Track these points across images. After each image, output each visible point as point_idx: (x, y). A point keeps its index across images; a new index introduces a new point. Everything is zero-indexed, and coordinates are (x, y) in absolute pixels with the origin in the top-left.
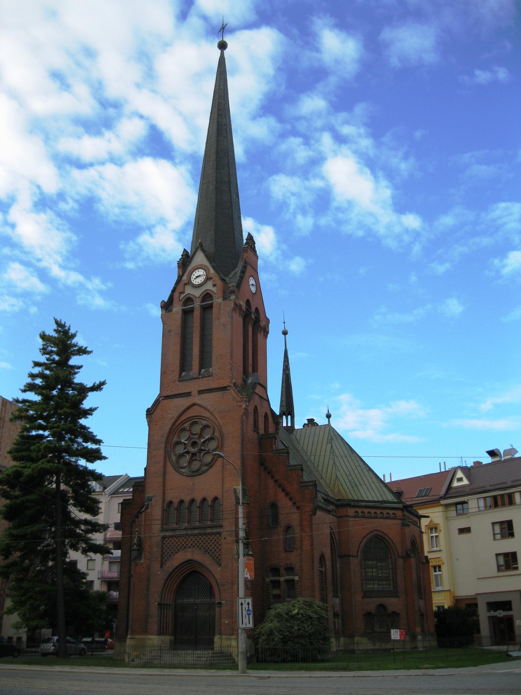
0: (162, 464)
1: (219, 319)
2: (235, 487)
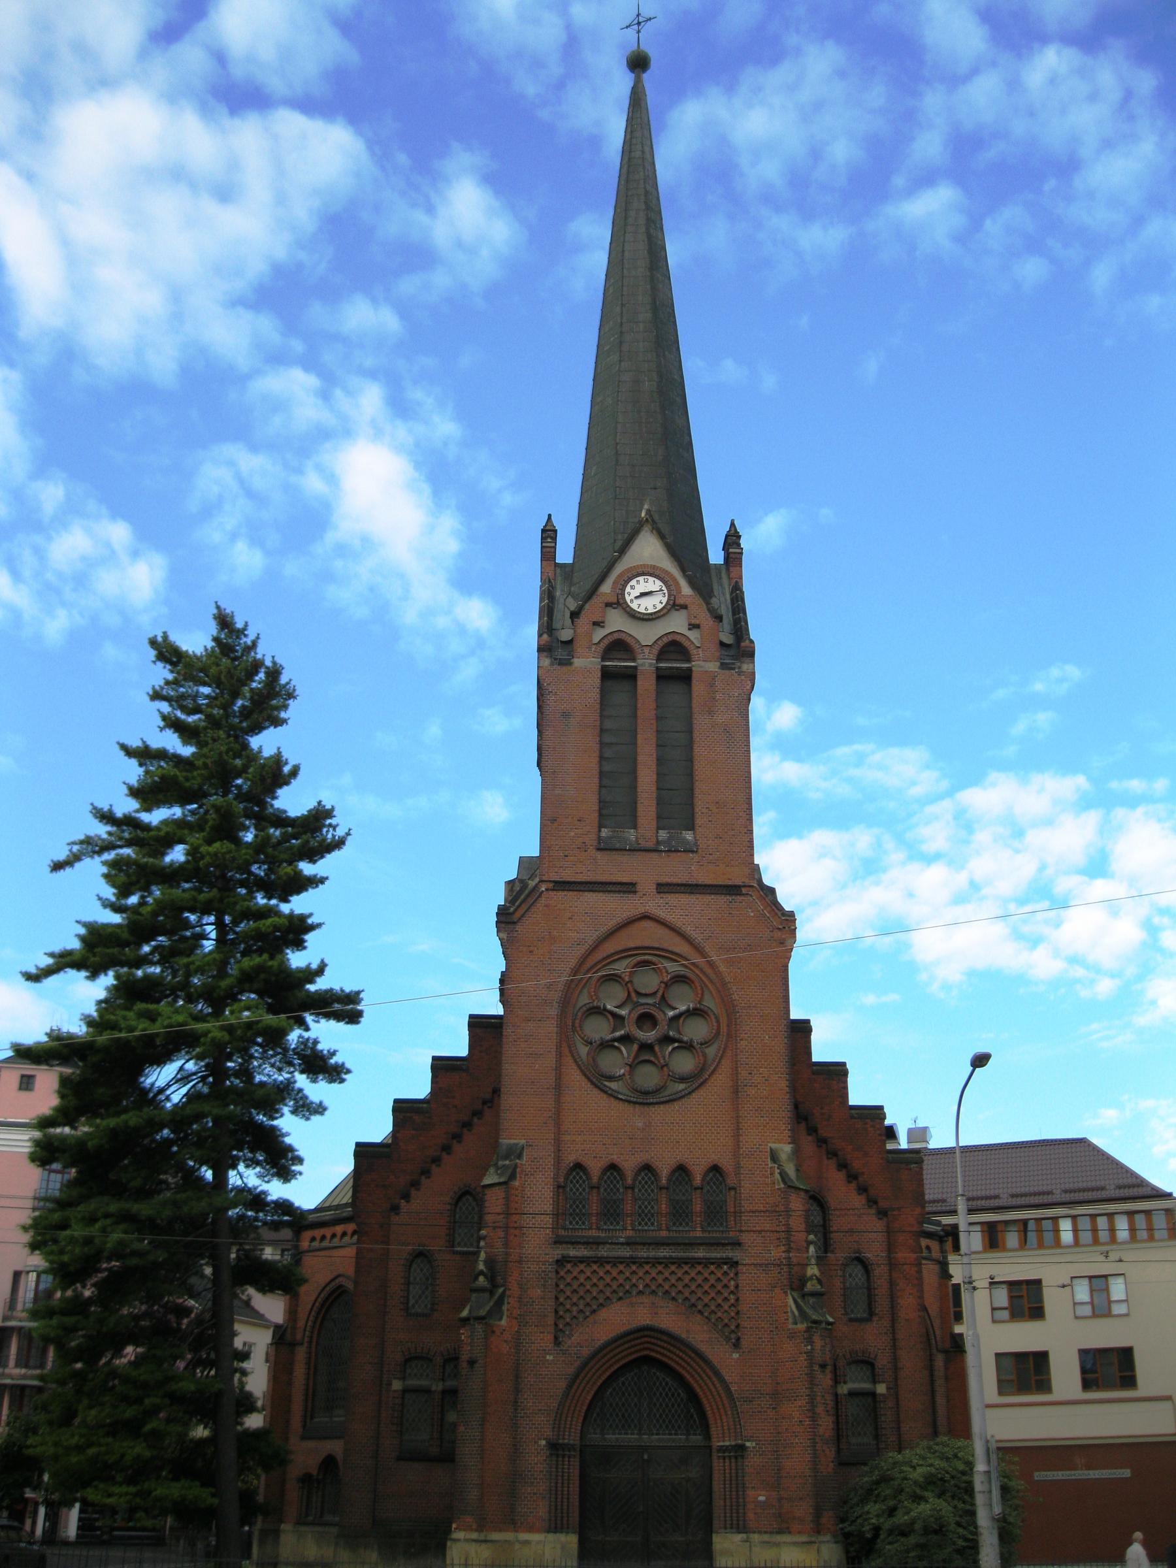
2: (773, 1146)
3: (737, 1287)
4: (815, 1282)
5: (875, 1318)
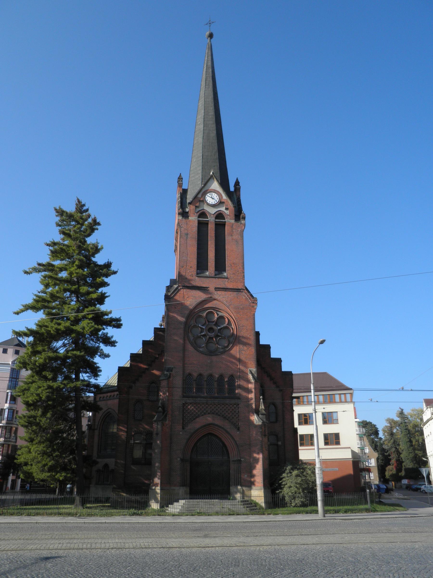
1: (232, 235)
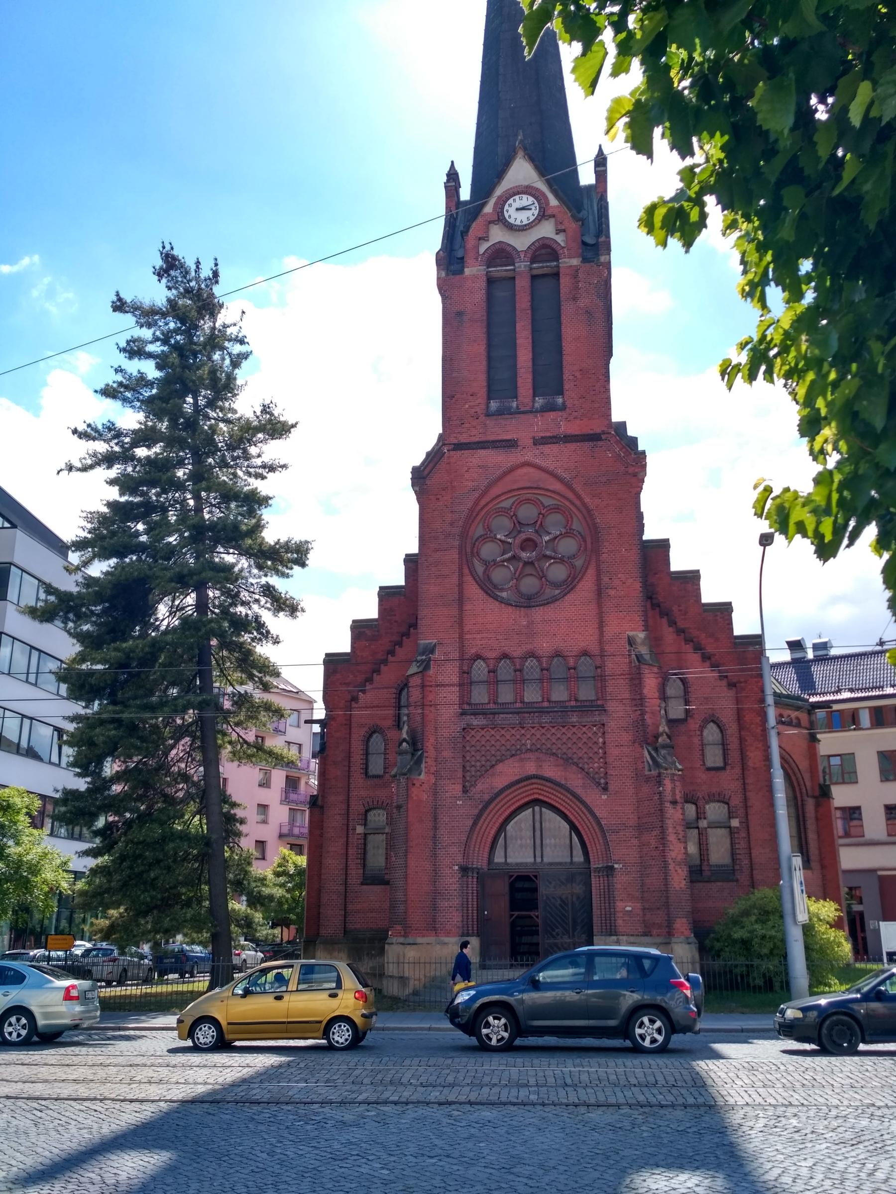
0: (455, 579)
1: (575, 299)
2: (631, 634)
3: (604, 743)
4: (665, 736)
5: (728, 767)
